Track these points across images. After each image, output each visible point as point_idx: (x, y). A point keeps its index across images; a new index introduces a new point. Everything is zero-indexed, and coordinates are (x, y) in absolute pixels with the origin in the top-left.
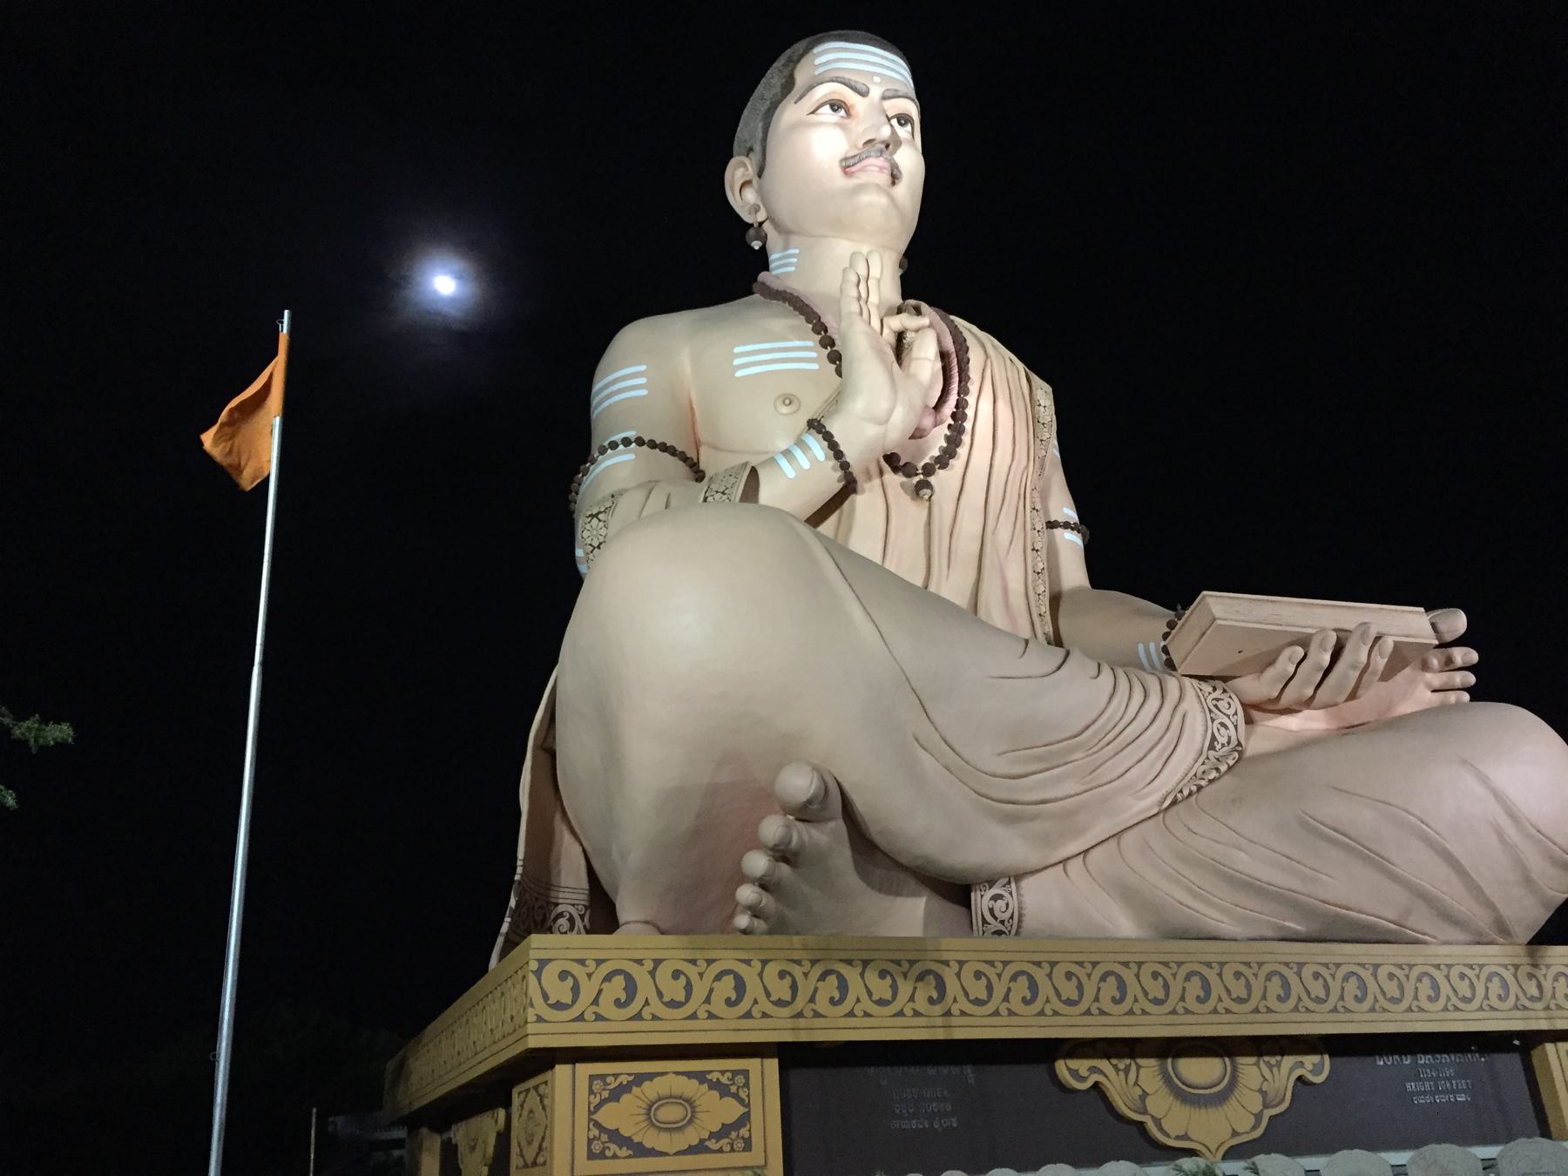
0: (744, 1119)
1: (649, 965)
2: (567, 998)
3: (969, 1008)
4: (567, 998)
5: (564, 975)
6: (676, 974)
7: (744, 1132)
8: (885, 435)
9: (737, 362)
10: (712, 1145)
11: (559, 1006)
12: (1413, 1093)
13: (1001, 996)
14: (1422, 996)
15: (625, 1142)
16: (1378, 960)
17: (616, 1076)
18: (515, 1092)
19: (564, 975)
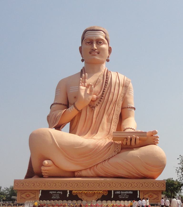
0: (35, 196)
1: (112, 183)
2: (126, 186)
3: (59, 187)
4: (126, 186)
5: (147, 184)
6: (17, 183)
7: (35, 198)
8: (131, 89)
9: (70, 90)
10: (32, 199)
11: (125, 186)
12: (119, 197)
13: (95, 186)
14: (97, 186)
15: (23, 198)
16: (145, 182)
17: (23, 192)
18: (74, 195)
19: (60, 183)
